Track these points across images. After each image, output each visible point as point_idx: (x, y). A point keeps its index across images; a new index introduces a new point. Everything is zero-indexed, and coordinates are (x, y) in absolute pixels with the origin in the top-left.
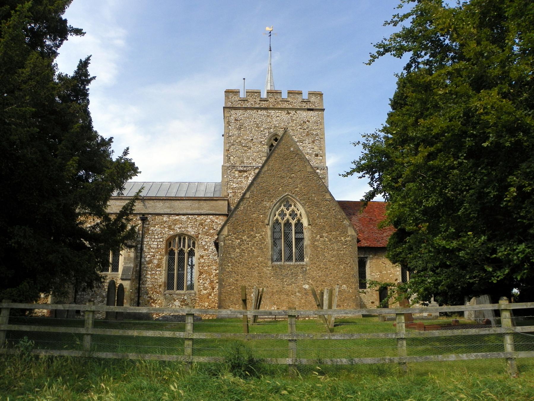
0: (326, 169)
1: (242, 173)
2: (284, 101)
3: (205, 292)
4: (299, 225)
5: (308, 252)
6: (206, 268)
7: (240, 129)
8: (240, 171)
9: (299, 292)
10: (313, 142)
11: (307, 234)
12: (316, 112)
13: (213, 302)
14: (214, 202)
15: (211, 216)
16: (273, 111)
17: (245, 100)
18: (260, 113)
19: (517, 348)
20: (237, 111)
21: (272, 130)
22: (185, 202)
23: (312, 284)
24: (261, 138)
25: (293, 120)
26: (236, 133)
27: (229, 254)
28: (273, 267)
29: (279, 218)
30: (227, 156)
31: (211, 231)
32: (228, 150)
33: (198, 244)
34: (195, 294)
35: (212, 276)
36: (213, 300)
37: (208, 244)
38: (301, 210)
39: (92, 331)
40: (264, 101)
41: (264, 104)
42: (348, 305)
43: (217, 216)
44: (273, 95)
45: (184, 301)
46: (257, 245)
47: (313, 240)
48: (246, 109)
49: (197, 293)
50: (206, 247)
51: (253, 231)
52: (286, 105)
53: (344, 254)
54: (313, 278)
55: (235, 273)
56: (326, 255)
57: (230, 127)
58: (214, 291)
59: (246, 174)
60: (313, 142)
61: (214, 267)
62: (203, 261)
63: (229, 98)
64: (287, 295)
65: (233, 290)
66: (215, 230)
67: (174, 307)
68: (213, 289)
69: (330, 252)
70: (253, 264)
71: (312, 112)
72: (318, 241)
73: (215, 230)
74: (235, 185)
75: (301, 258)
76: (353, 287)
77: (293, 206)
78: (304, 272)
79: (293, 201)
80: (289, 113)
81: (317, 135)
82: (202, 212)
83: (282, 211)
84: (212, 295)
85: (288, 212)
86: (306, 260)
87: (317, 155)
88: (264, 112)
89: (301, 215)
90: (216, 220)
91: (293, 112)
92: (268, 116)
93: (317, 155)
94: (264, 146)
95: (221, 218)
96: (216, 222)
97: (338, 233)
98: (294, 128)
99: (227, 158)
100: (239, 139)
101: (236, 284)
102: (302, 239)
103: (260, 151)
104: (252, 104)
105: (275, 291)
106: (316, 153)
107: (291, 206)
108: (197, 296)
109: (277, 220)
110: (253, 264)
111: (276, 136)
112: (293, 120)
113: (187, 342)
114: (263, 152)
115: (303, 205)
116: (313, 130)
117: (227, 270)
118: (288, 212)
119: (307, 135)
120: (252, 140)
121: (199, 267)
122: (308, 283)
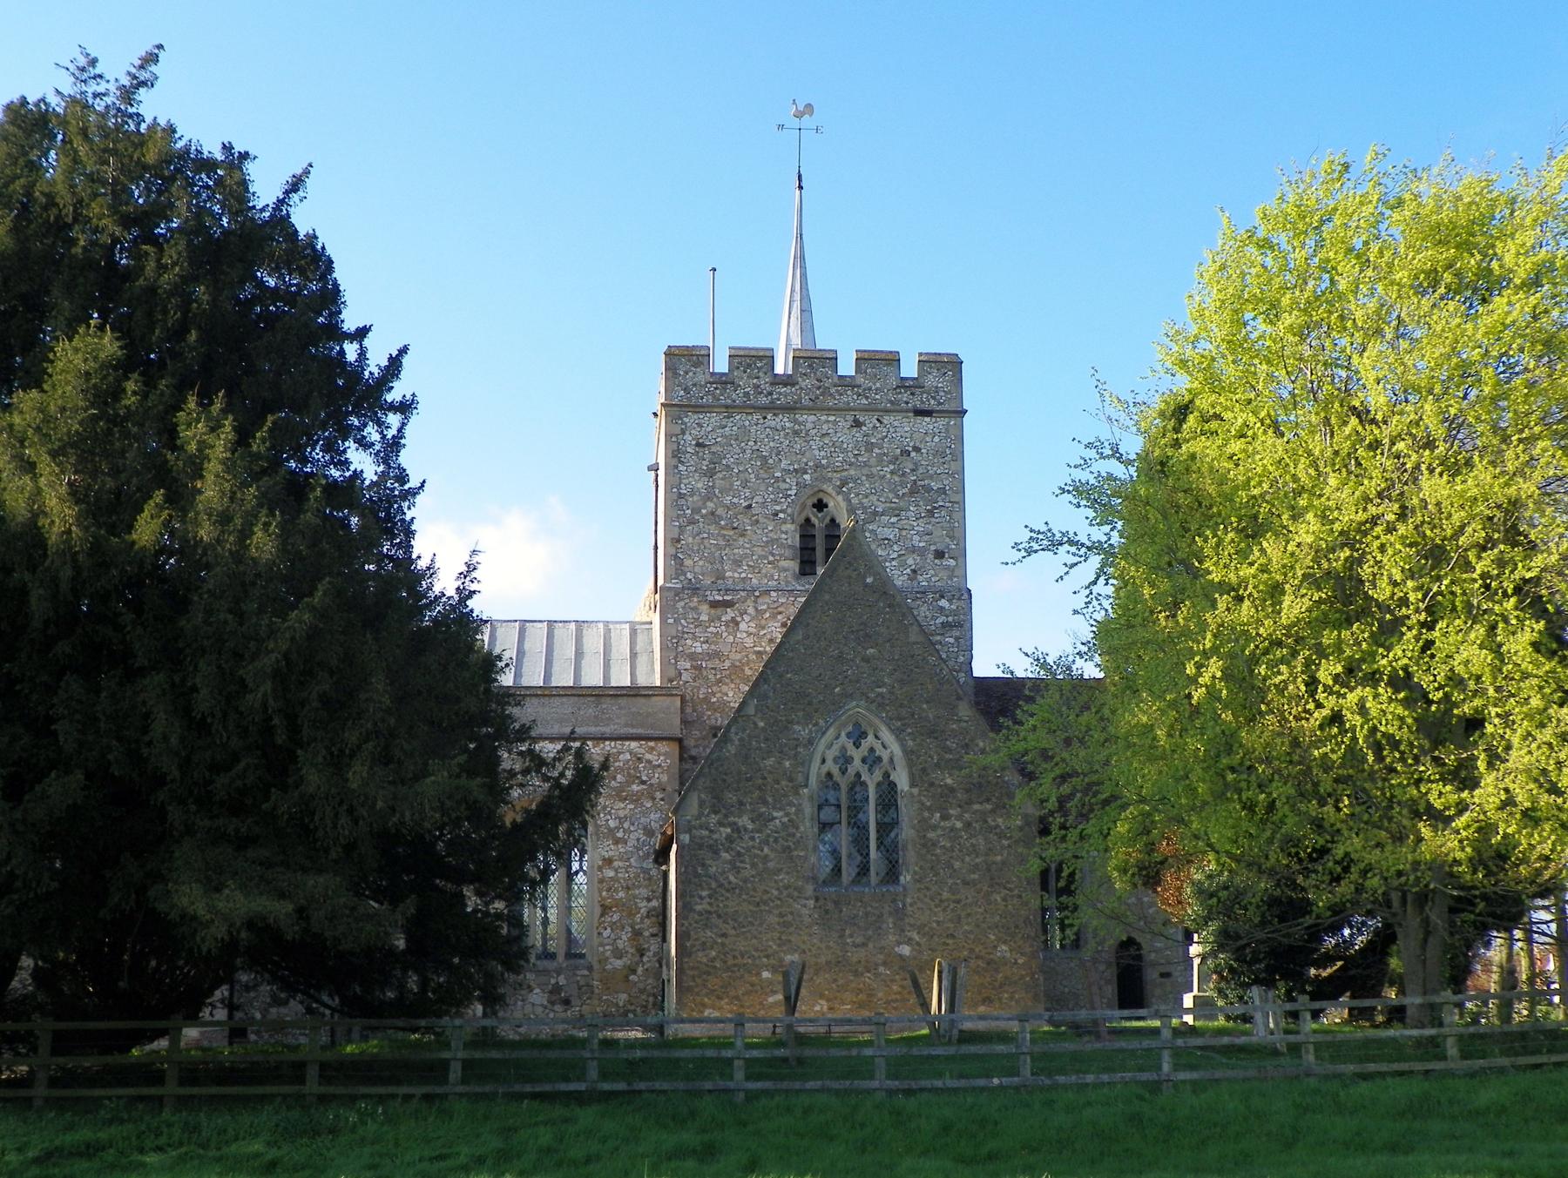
0: (966, 596)
1: (719, 611)
2: (845, 383)
3: (618, 963)
4: (888, 792)
5: (910, 858)
6: (621, 894)
7: (711, 473)
8: (714, 605)
9: (885, 964)
10: (931, 513)
11: (907, 812)
12: (942, 422)
13: (642, 991)
14: (642, 700)
15: (634, 744)
16: (812, 418)
17: (726, 383)
18: (773, 424)
19: (1176, 1067)
20: (704, 418)
21: (807, 477)
22: (557, 701)
23: (918, 944)
24: (775, 502)
25: (870, 447)
26: (700, 485)
27: (703, 865)
28: (817, 899)
29: (835, 771)
30: (676, 557)
31: (635, 787)
32: (678, 541)
33: (597, 826)
34: (590, 968)
35: (638, 918)
36: (641, 986)
37: (626, 825)
38: (890, 745)
39: (460, 1055)
40: (785, 385)
41: (784, 394)
42: (1012, 998)
43: (652, 744)
44: (810, 366)
45: (556, 989)
46: (776, 840)
47: (924, 826)
48: (730, 409)
49: (596, 966)
50: (620, 835)
51: (765, 803)
52: (849, 397)
53: (1003, 863)
54: (920, 929)
55: (719, 916)
56: (957, 865)
57: (681, 468)
58: (645, 959)
59: (730, 613)
60: (931, 513)
61: (644, 892)
62: (611, 874)
63: (676, 374)
64: (856, 973)
65: (713, 960)
66: (643, 783)
67: (528, 1008)
68: (642, 955)
69: (967, 859)
70: (766, 892)
71: (927, 419)
72: (934, 828)
73: (643, 783)
74: (698, 648)
75: (892, 874)
76: (1028, 950)
77: (870, 738)
78: (899, 914)
79: (871, 724)
80: (857, 424)
81: (942, 491)
82: (607, 730)
83: (844, 749)
84: (640, 970)
85: (857, 755)
86: (906, 878)
87: (940, 555)
88: (784, 421)
89: (891, 760)
90: (648, 756)
91: (870, 421)
92: (796, 433)
93: (940, 555)
94: (784, 528)
95: (663, 747)
96: (649, 762)
97: (989, 807)
98: (874, 470)
99: (676, 563)
100: (710, 505)
101: (723, 944)
102: (895, 823)
103: (772, 541)
104: (747, 394)
105: (823, 959)
106: (940, 547)
107: (864, 735)
108: (596, 975)
109: (829, 775)
110: (766, 892)
111: (821, 495)
112: (870, 447)
113: (736, 1063)
114: (782, 546)
115: (898, 733)
116: (931, 477)
117: (698, 908)
118: (857, 755)
119: (912, 492)
120: (750, 506)
121: (600, 891)
122: (909, 941)
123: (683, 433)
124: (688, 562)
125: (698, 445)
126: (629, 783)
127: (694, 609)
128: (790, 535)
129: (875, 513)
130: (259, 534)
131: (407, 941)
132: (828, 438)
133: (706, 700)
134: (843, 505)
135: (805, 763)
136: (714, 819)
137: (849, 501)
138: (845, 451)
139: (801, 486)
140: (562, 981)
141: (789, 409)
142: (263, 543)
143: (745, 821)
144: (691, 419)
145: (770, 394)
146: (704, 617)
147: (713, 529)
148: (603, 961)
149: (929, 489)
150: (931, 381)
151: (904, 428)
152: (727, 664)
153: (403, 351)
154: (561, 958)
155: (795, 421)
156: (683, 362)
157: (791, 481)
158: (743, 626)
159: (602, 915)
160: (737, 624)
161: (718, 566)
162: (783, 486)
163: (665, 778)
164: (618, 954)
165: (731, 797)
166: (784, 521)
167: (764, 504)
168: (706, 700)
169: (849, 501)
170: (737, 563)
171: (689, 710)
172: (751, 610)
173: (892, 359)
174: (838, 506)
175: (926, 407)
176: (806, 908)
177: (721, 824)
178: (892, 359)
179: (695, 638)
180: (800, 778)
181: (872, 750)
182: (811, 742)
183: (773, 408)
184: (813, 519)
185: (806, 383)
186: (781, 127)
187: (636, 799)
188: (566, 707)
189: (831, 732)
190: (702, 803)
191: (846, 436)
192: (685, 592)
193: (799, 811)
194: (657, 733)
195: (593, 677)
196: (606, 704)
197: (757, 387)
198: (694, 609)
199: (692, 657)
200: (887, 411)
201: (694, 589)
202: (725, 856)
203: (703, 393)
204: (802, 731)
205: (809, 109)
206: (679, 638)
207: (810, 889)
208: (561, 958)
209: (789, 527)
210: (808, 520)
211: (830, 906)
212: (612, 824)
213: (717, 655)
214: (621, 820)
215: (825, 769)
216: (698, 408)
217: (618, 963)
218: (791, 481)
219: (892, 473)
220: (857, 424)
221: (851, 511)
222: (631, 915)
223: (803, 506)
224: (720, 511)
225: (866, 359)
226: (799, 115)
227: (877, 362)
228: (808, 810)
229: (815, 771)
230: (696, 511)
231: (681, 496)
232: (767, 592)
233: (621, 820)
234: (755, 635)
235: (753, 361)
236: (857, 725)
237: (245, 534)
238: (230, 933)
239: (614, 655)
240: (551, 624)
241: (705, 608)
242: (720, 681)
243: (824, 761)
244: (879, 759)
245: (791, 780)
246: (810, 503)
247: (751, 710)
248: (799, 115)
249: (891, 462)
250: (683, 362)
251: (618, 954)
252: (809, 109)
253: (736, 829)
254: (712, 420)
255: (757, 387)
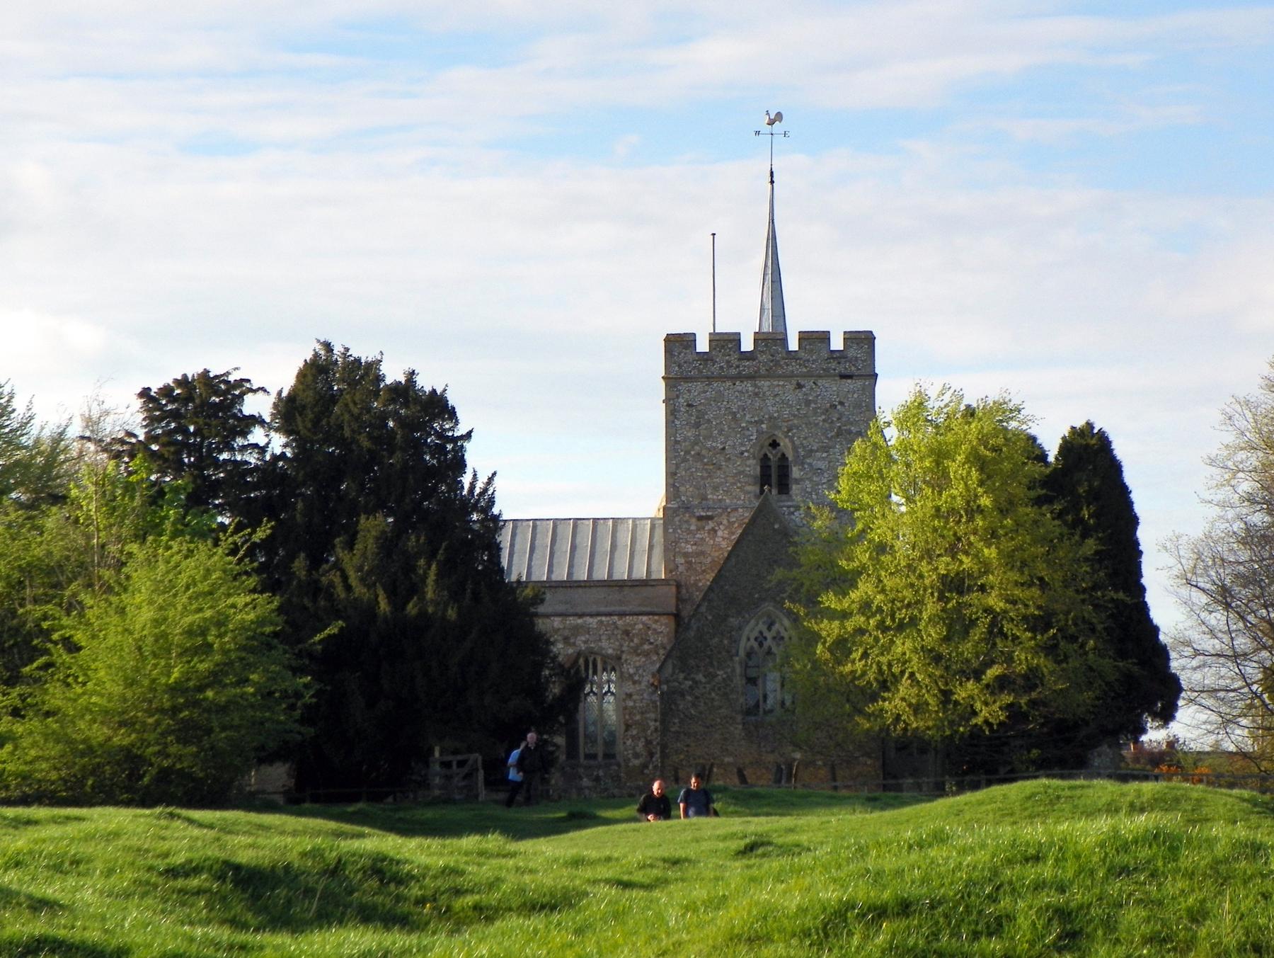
1: (703, 523)
7: (697, 425)
8: (700, 518)
12: (859, 383)
15: (645, 618)
16: (768, 383)
22: (594, 590)
24: (742, 444)
25: (808, 403)
30: (674, 486)
50: (636, 678)
52: (794, 367)
57: (677, 422)
59: (711, 524)
61: (652, 716)
74: (690, 549)
80: (799, 386)
84: (651, 767)
88: (748, 386)
91: (809, 383)
94: (749, 462)
95: (664, 619)
98: (811, 419)
100: (697, 448)
103: (740, 473)
104: (721, 368)
112: (808, 403)
114: (746, 476)
116: (851, 424)
119: (838, 435)
120: (724, 449)
123: (678, 397)
124: (682, 489)
125: (689, 405)
126: (642, 644)
127: (687, 522)
128: (753, 468)
129: (811, 451)
130: (450, 611)
131: (459, 614)
132: (779, 398)
133: (695, 584)
134: (789, 445)
135: (735, 641)
136: (682, 676)
137: (793, 442)
138: (791, 406)
139: (760, 432)
140: (601, 773)
141: (751, 377)
142: (452, 614)
143: (700, 677)
144: (683, 387)
145: (738, 367)
146: (693, 528)
147: (699, 465)
148: (627, 760)
149: (850, 432)
150: (851, 353)
151: (832, 389)
152: (709, 559)
153: (494, 474)
154: (600, 758)
155: (756, 386)
156: (678, 344)
157: (753, 429)
158: (720, 533)
159: (626, 730)
160: (716, 531)
161: (702, 491)
162: (747, 433)
163: (665, 641)
164: (637, 756)
165: (692, 662)
166: (748, 458)
167: (734, 447)
168: (695, 584)
169: (793, 442)
170: (716, 488)
171: (684, 591)
172: (725, 522)
173: (824, 337)
174: (785, 445)
175: (848, 372)
176: (737, 730)
177: (685, 679)
178: (824, 337)
179: (687, 542)
180: (734, 651)
181: (778, 632)
182: (740, 628)
183: (740, 377)
184: (770, 455)
185: (763, 358)
186: (758, 133)
187: (647, 654)
188: (600, 594)
189: (753, 622)
190: (674, 666)
191: (792, 396)
192: (682, 505)
193: (733, 670)
194: (660, 610)
195: (622, 573)
196: (626, 590)
197: (728, 362)
198: (687, 522)
199: (686, 555)
200: (820, 376)
201: (687, 508)
202: (689, 698)
203: (694, 368)
204: (733, 621)
205: (779, 116)
206: (676, 543)
207: (739, 718)
208: (600, 758)
209: (751, 462)
210: (766, 455)
211: (752, 728)
212: (631, 671)
213: (703, 553)
214: (637, 668)
215: (749, 644)
216: (687, 379)
217: (637, 762)
218: (753, 429)
219: (824, 421)
220: (799, 386)
221: (795, 448)
222: (644, 730)
223: (762, 447)
224: (704, 452)
225: (805, 337)
226: (771, 123)
227: (815, 340)
228: (738, 670)
229: (743, 645)
230: (687, 452)
231: (677, 442)
232: (736, 509)
233: (637, 668)
234: (723, 539)
235: (725, 342)
236: (769, 616)
237: (445, 610)
238: (1081, 907)
239: (638, 547)
240: (595, 520)
241: (694, 520)
242: (704, 571)
243: (748, 639)
244: (782, 638)
245: (728, 652)
246: (767, 443)
247: (703, 609)
248: (771, 123)
249: (823, 413)
250: (678, 344)
251: (637, 756)
252: (779, 116)
253: (695, 682)
254: (699, 386)
255: (728, 362)
